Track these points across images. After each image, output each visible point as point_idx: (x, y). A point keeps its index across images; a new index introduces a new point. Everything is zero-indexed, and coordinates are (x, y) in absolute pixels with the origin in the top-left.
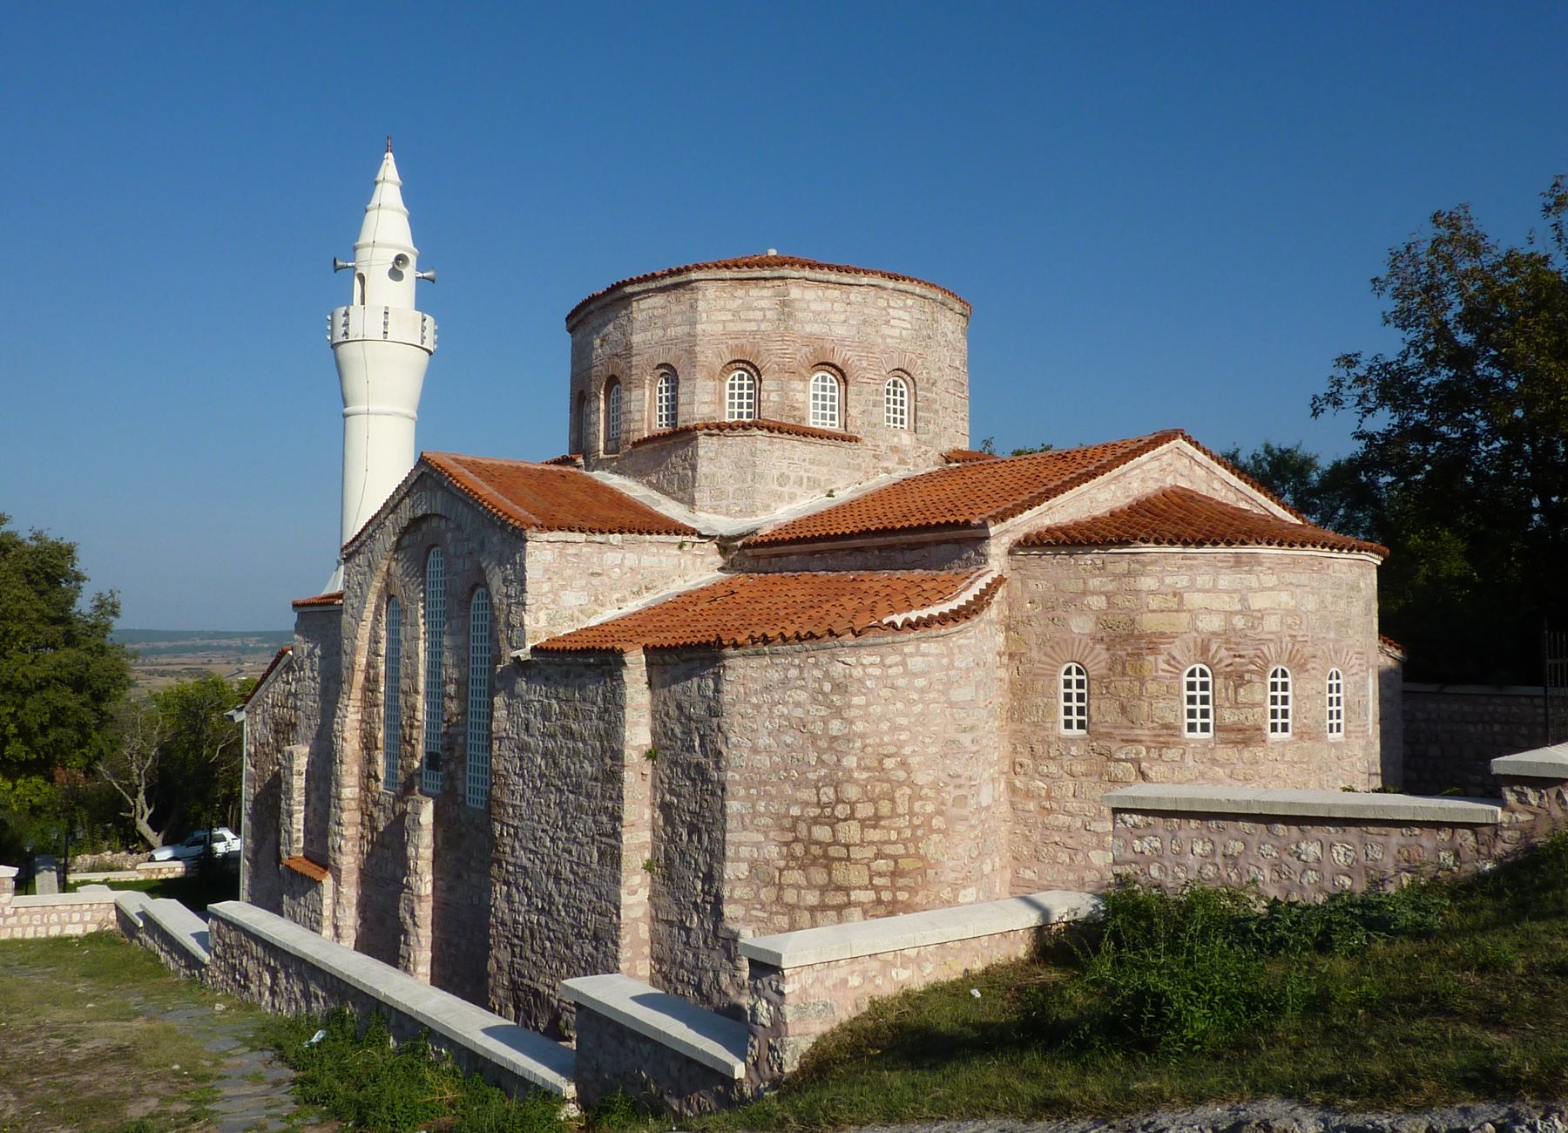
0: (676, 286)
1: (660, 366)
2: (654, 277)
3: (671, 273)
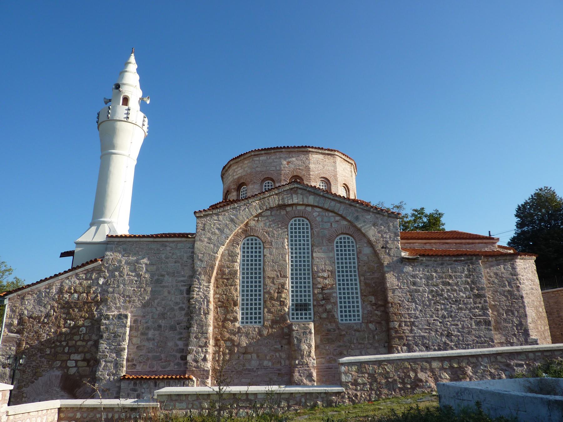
0: (328, 154)
1: (322, 177)
2: (322, 149)
3: (329, 150)
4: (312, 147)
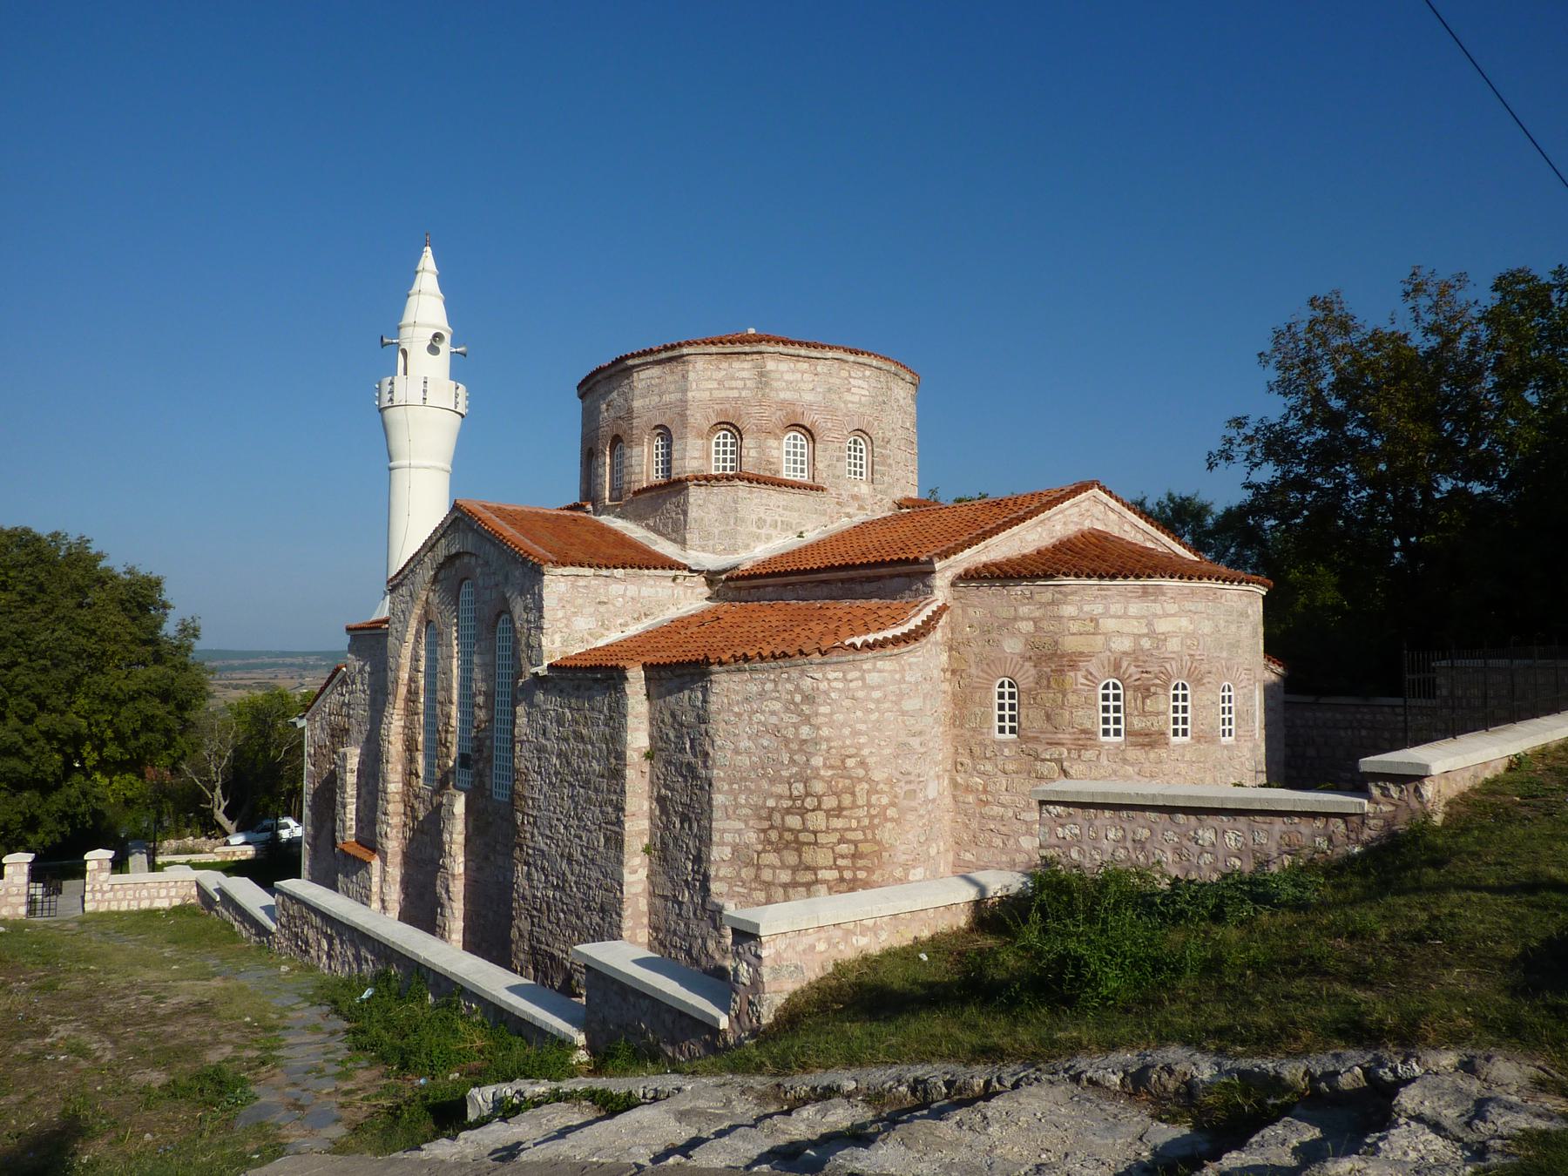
0: (670, 359)
1: (657, 427)
2: (651, 352)
3: (666, 349)
4: (633, 356)
